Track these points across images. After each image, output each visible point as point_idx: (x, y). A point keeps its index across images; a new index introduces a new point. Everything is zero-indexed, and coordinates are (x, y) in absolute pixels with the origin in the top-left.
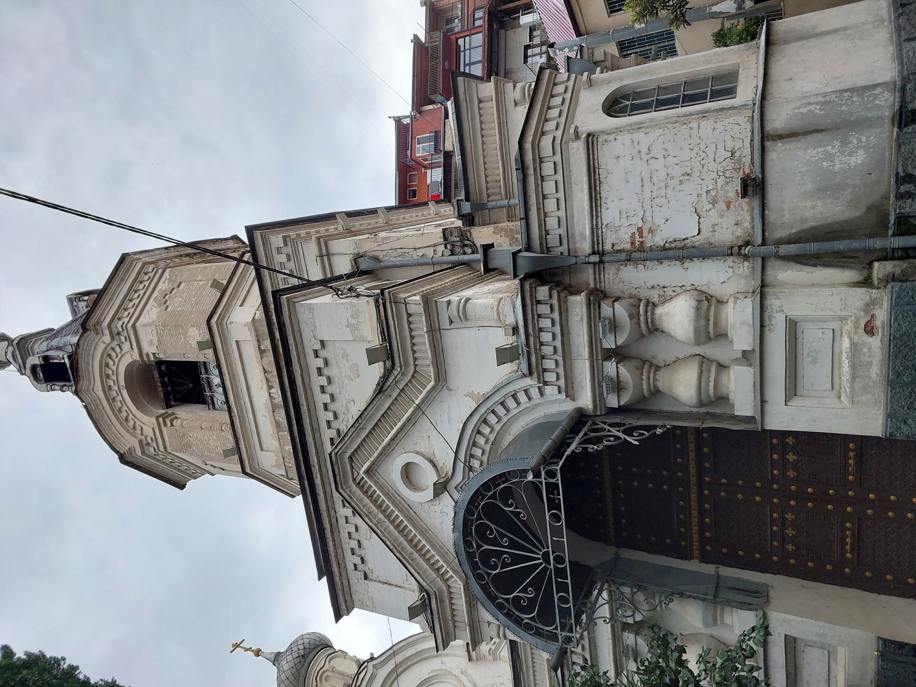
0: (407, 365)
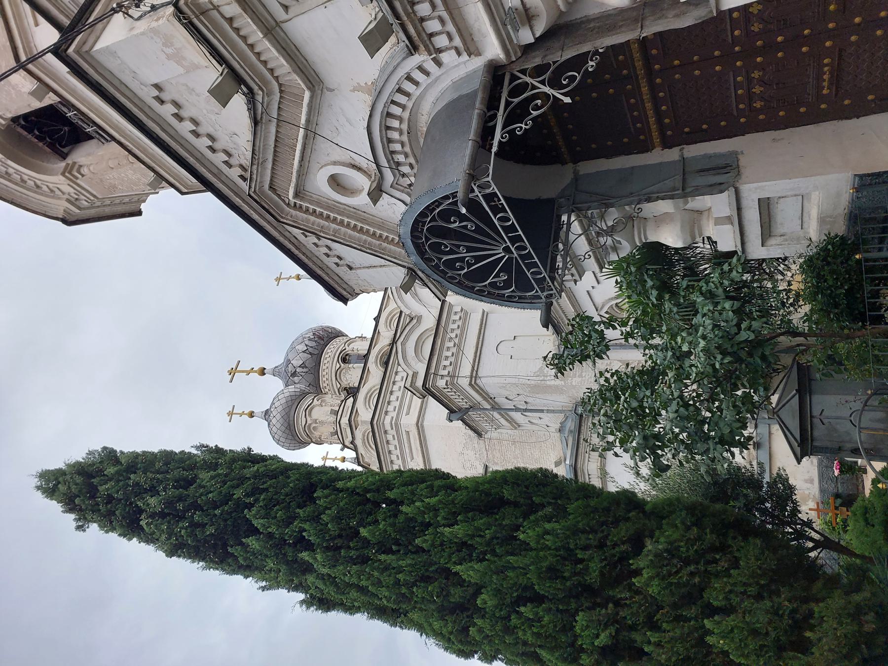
0: (265, 82)
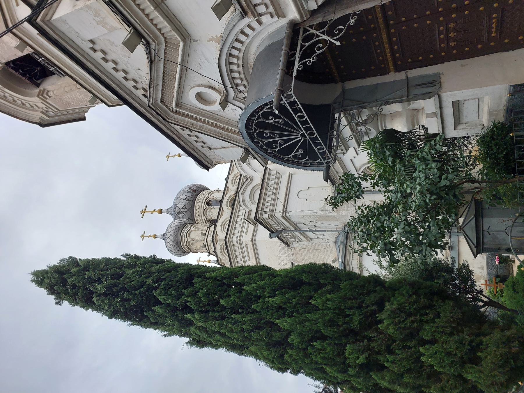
0: (157, 37)
